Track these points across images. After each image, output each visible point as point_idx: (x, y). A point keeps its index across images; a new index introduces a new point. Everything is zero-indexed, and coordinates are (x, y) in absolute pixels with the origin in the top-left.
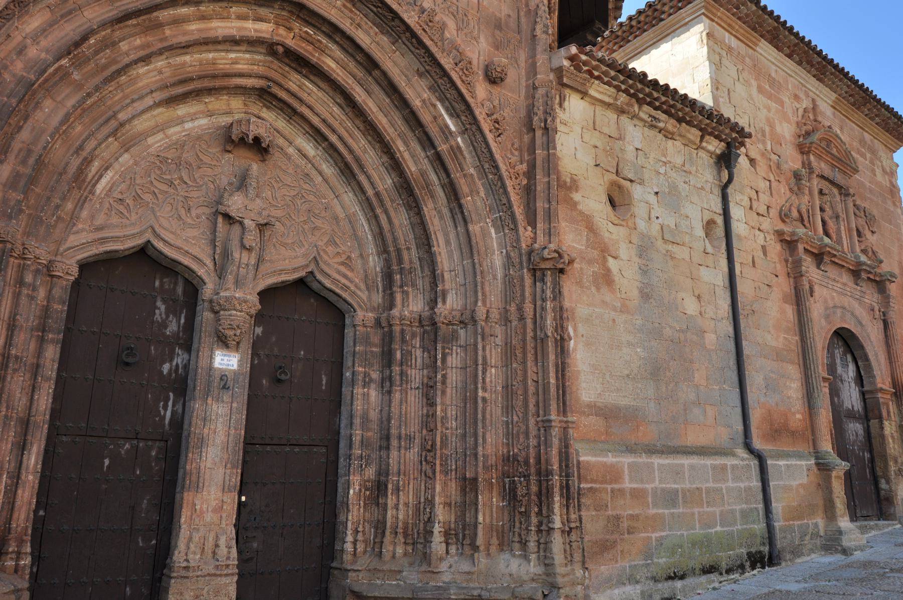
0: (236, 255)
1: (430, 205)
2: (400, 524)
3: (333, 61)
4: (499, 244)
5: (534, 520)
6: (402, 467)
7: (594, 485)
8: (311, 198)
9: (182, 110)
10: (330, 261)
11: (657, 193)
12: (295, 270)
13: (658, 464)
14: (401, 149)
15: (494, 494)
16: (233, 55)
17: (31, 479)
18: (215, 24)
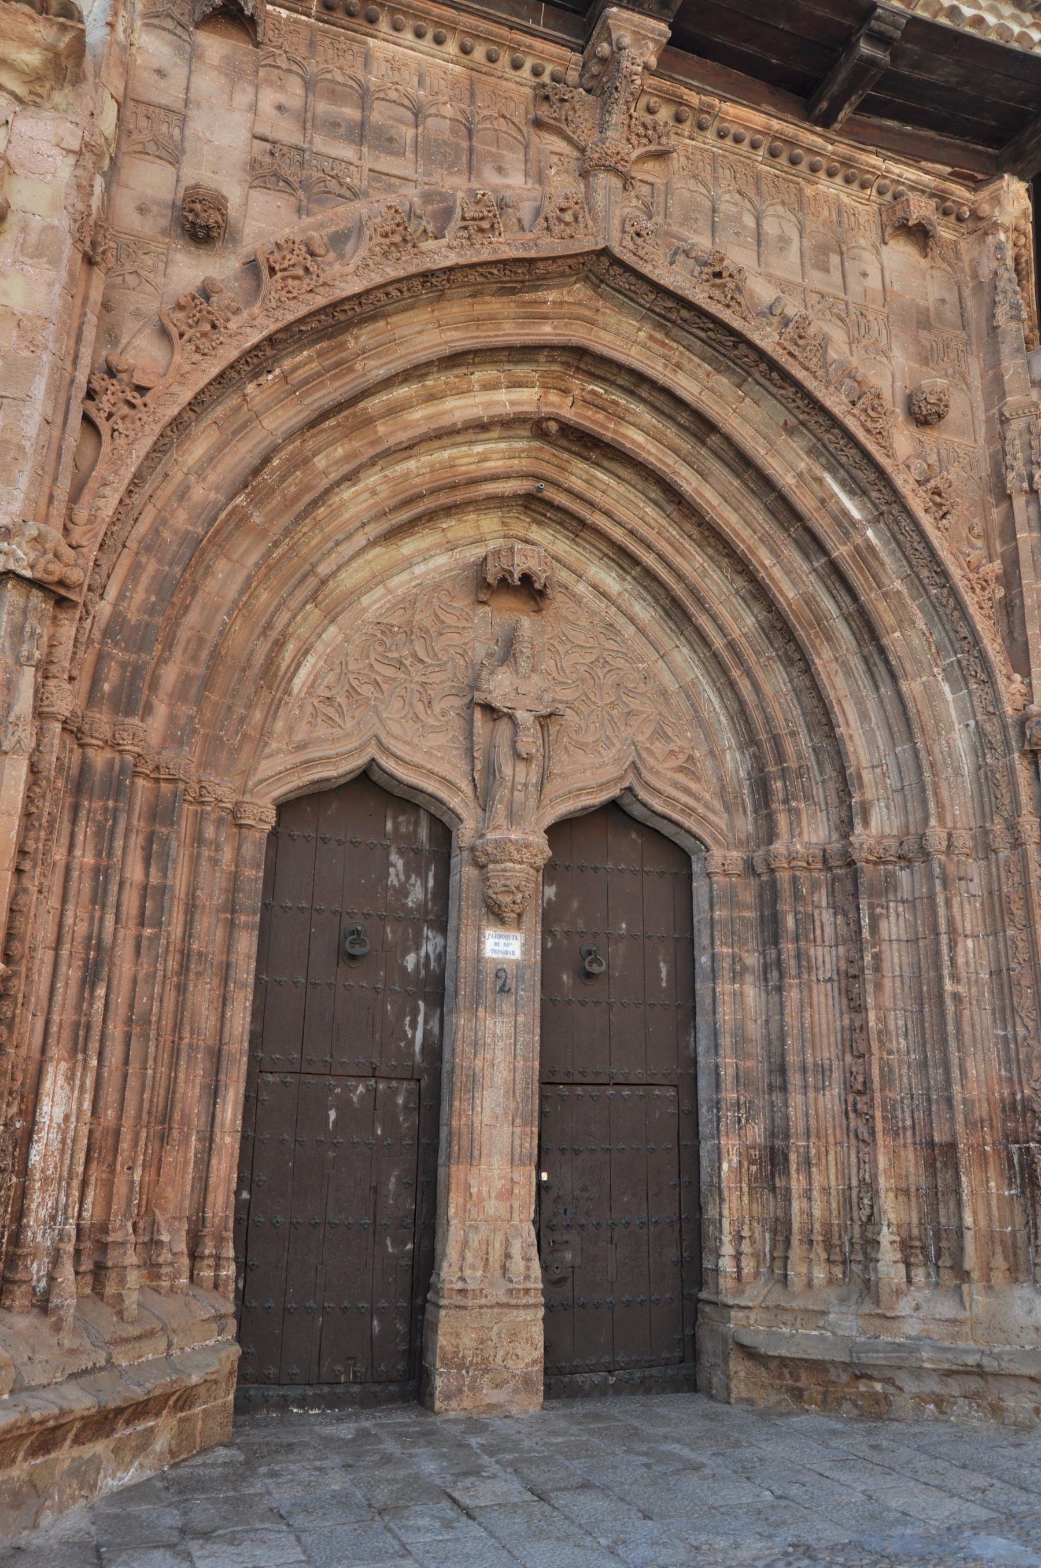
0: (507, 770)
1: (827, 653)
2: (817, 1226)
3: (639, 431)
6: (813, 1123)
8: (620, 663)
9: (409, 546)
10: (659, 767)
12: (602, 787)
14: (767, 562)
15: (992, 1173)
16: (479, 448)
17: (228, 1141)
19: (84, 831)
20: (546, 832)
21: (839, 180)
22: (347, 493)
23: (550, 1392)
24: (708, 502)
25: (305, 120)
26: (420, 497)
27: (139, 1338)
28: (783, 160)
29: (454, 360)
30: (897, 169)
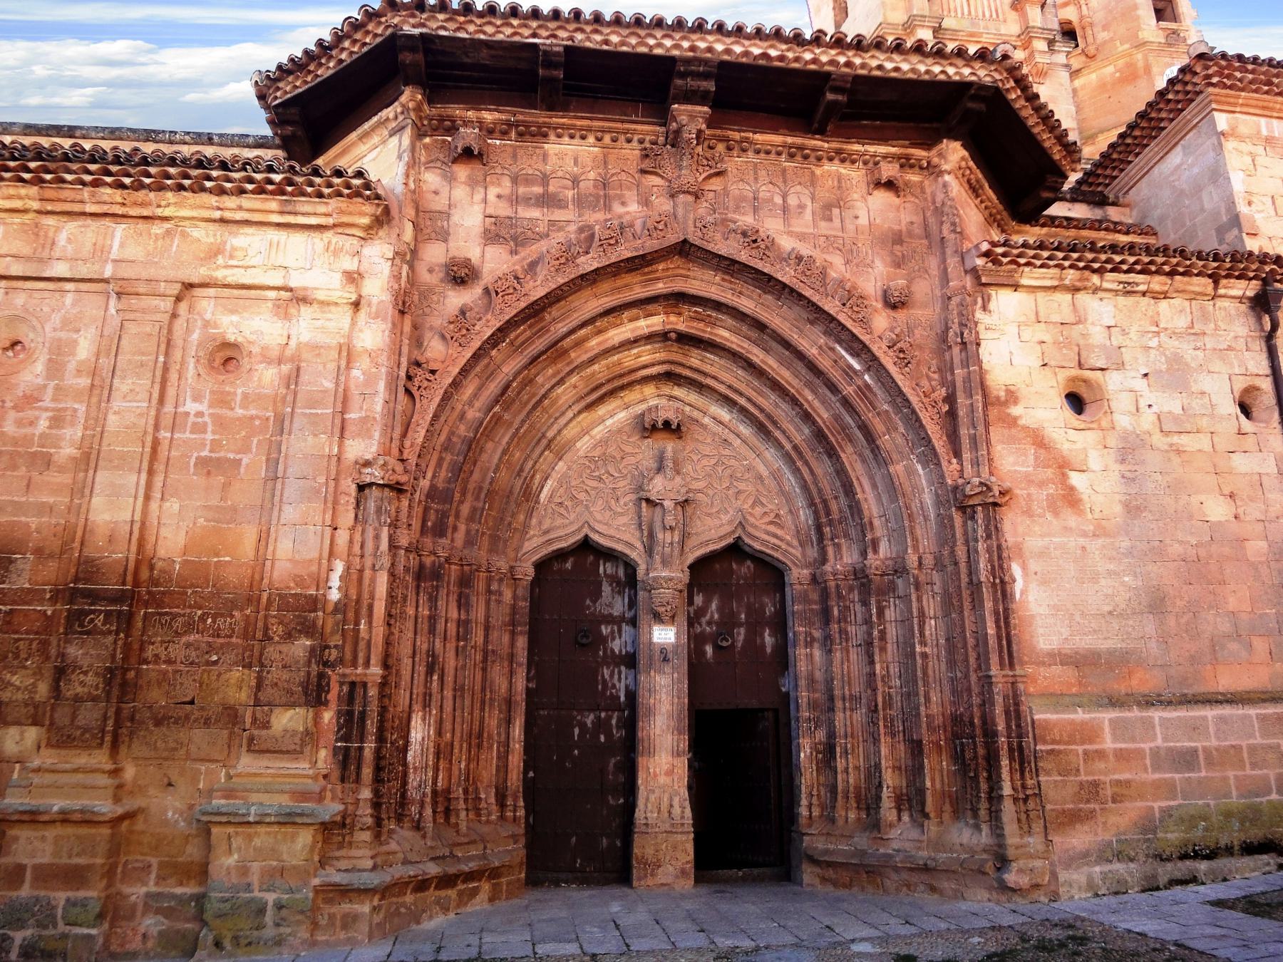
0: (660, 536)
1: (849, 449)
2: (851, 789)
3: (724, 334)
4: (928, 481)
5: (984, 786)
6: (849, 730)
7: (1057, 747)
8: (733, 462)
9: (602, 410)
10: (757, 523)
11: (1146, 375)
12: (721, 538)
13: (1160, 718)
14: (810, 398)
15: (944, 757)
16: (635, 351)
17: (517, 747)
18: (612, 333)
19: (423, 598)
20: (690, 567)
21: (836, 161)
22: (560, 390)
23: (698, 881)
24: (770, 367)
25: (515, 200)
26: (602, 385)
27: (468, 843)
28: (799, 158)
29: (608, 312)
30: (872, 149)
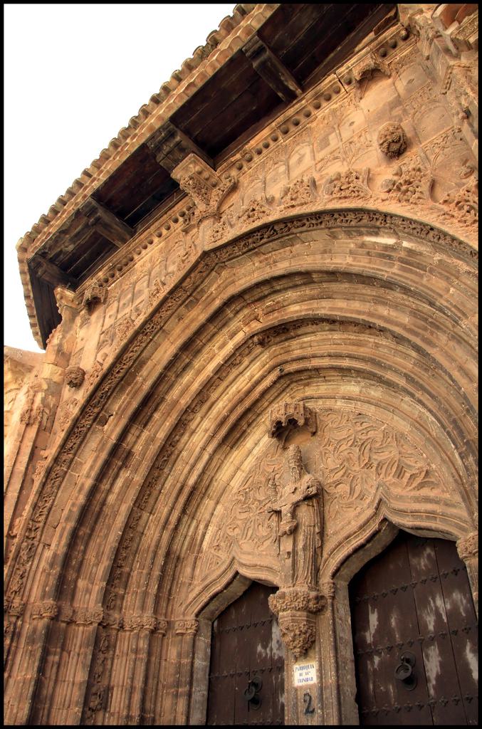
3: (294, 305)
12: (362, 527)
21: (324, 104)
